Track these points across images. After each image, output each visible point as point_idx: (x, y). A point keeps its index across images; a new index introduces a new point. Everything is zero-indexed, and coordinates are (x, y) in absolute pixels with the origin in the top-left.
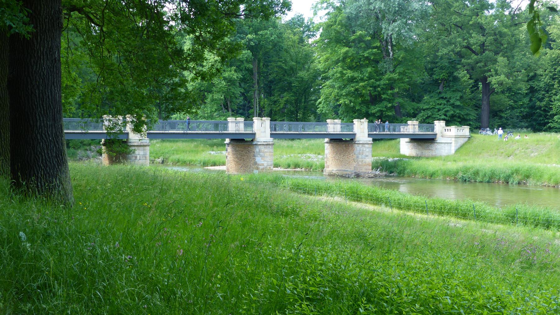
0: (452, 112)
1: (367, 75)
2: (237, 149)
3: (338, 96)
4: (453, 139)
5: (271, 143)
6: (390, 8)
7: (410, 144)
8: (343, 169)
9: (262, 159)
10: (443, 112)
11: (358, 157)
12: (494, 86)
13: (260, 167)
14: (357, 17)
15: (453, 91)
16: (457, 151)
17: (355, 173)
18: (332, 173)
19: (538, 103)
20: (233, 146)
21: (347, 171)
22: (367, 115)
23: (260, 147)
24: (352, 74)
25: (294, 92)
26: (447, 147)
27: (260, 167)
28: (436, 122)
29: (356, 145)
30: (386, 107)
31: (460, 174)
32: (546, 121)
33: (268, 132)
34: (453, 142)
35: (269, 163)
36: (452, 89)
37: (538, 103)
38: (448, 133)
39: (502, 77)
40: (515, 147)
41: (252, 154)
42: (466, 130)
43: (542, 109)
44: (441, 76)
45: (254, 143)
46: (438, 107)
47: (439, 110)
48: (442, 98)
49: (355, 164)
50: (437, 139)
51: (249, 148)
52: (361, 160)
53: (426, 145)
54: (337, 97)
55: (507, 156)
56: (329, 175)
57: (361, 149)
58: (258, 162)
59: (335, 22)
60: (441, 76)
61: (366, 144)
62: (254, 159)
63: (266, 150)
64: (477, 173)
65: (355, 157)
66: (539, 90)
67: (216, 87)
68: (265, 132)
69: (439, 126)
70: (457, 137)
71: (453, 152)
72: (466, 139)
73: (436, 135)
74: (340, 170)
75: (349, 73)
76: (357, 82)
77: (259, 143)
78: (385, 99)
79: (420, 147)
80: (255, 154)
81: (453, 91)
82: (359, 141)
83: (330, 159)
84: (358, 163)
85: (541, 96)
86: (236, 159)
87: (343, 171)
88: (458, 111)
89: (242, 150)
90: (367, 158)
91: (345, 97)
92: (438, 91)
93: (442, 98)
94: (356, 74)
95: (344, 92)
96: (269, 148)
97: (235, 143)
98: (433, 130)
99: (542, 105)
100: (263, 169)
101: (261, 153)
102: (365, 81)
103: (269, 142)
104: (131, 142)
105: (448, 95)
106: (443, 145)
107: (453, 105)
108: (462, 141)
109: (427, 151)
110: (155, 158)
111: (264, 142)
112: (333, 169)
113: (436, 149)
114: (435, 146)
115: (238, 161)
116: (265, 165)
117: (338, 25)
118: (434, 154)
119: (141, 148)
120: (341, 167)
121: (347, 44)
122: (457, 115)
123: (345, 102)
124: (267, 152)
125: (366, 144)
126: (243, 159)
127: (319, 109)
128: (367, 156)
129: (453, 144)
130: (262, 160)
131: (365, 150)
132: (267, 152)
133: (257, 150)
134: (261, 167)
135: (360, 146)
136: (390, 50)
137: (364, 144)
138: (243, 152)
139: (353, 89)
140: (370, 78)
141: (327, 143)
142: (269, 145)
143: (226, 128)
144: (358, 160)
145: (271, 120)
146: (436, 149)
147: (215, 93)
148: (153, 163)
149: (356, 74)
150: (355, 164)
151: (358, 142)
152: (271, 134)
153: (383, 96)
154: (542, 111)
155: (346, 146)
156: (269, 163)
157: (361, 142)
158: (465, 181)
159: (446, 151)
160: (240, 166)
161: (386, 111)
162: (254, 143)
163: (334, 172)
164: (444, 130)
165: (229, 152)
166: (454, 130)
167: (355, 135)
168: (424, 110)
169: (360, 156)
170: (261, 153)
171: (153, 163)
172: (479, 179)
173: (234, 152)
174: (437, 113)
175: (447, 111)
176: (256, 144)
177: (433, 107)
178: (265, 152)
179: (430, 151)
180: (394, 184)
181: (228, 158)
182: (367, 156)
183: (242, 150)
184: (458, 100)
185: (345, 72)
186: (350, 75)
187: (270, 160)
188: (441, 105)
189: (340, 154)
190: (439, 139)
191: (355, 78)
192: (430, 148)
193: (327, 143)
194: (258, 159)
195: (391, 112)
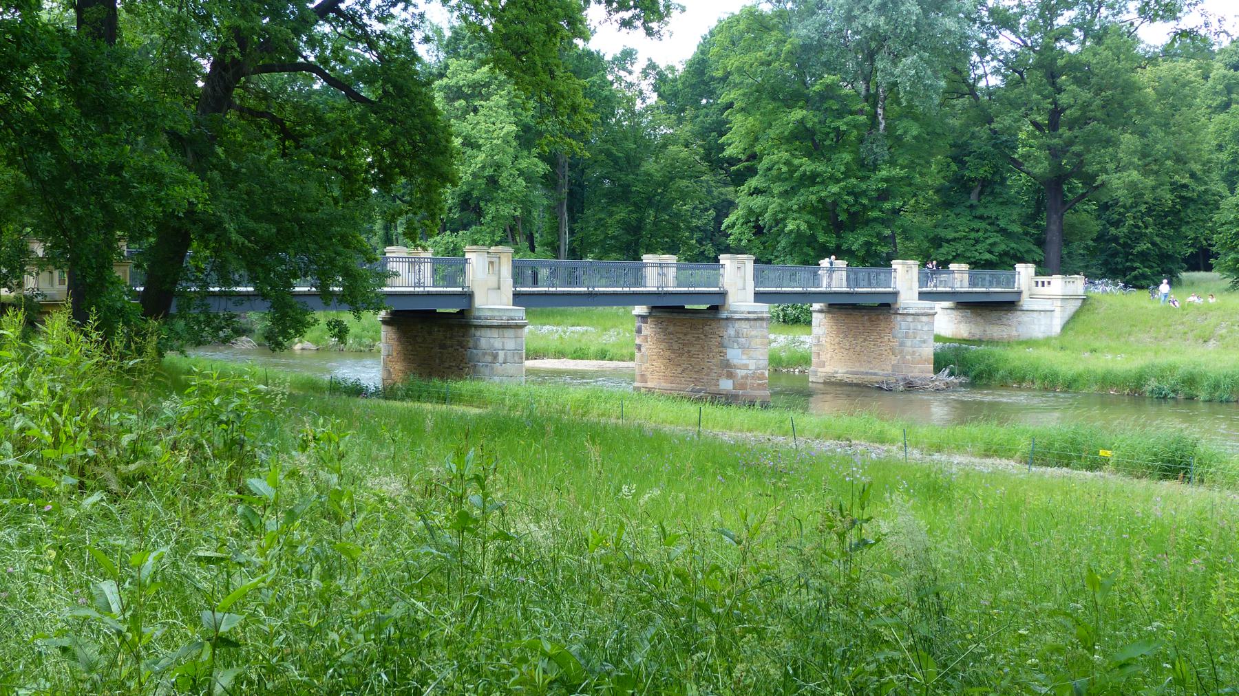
0: (1003, 247)
1: (843, 168)
2: (671, 328)
3: (781, 211)
4: (1059, 303)
5: (765, 315)
6: (896, 28)
7: (955, 313)
8: (862, 370)
9: (743, 353)
10: (985, 246)
11: (902, 344)
12: (1119, 192)
13: (738, 371)
14: (819, 47)
15: (1002, 203)
16: (1065, 328)
17: (905, 379)
18: (833, 379)
19: (1113, 230)
20: (659, 322)
21: (875, 374)
22: (839, 253)
23: (737, 324)
24: (813, 167)
25: (635, 204)
26: (1043, 320)
27: (738, 371)
28: (1020, 267)
29: (899, 318)
30: (878, 235)
31: (1153, 384)
32: (1128, 264)
33: (508, 288)
34: (1058, 310)
35: (761, 362)
36: (1001, 200)
37: (1113, 230)
38: (1046, 290)
39: (1135, 175)
40: (1212, 321)
41: (714, 342)
42: (1077, 284)
43: (1121, 241)
44: (981, 172)
45: (724, 315)
46: (973, 235)
47: (977, 241)
48: (981, 218)
49: (894, 360)
50: (1021, 303)
51: (707, 328)
52: (910, 350)
53: (995, 314)
54: (780, 216)
55: (1201, 341)
56: (825, 383)
57: (912, 326)
58: (734, 361)
59: (778, 55)
60: (981, 172)
61: (922, 315)
62: (724, 354)
63: (753, 333)
64: (1191, 381)
65: (895, 343)
66: (1111, 205)
67: (503, 191)
68: (499, 288)
69: (1025, 273)
70: (1065, 298)
71: (1057, 329)
72: (1079, 303)
73: (1019, 293)
74: (856, 373)
75: (807, 165)
76: (823, 182)
77: (737, 316)
78: (875, 220)
79: (979, 319)
80: (726, 342)
81: (1002, 203)
82: (905, 308)
83: (829, 347)
84: (903, 357)
85: (1116, 217)
86: (667, 354)
87: (862, 373)
88: (1013, 245)
89: (685, 331)
90: (924, 345)
91: (795, 215)
92: (968, 204)
93: (981, 218)
94: (820, 167)
95: (794, 203)
96: (761, 327)
97: (667, 315)
98: (1010, 281)
99: (1121, 235)
100: (746, 377)
101: (742, 340)
102: (838, 181)
103: (762, 312)
104: (479, 318)
105: (993, 211)
106: (1035, 314)
107: (1003, 231)
108: (1074, 306)
109: (996, 328)
110: (374, 340)
111: (749, 313)
112: (836, 369)
113: (1020, 323)
114: (1015, 318)
115: (673, 356)
116: (752, 367)
117: (785, 60)
118: (1014, 333)
119: (510, 333)
120: (857, 364)
121: (808, 102)
122: (1012, 251)
123: (798, 226)
124: (756, 337)
125: (922, 315)
126: (689, 352)
127: (732, 237)
128: (924, 342)
129: (1058, 313)
130: (744, 357)
131: (920, 327)
132: (756, 337)
133: (731, 332)
134: (741, 373)
135: (910, 319)
136: (880, 118)
137: (918, 315)
138: (688, 337)
139: (814, 197)
140: (847, 175)
141: (820, 311)
142: (761, 319)
143: (640, 281)
144: (902, 351)
145: (756, 262)
146: (1020, 323)
147: (501, 203)
148: (370, 350)
149: (820, 167)
150: (894, 360)
151: (905, 312)
152: (920, 293)
153: (874, 214)
154: (1119, 244)
155: (870, 320)
156: (761, 362)
157: (911, 311)
158: (1165, 397)
159: (1043, 328)
160: (680, 370)
161: (879, 244)
162: (724, 315)
163: (839, 376)
164: (1034, 284)
165: (646, 337)
166: (1057, 284)
167: (723, 295)
168: (948, 241)
169: (909, 343)
170: (742, 340)
171: (370, 350)
172: (1203, 395)
173: (662, 336)
174: (973, 249)
175: (994, 244)
176: (727, 319)
177: (965, 236)
178: (751, 337)
179: (1003, 328)
180: (993, 406)
181: (643, 349)
182: (924, 342)
183: (685, 331)
184: (1014, 221)
185: (796, 162)
186: (808, 169)
187: (762, 355)
188: (978, 231)
189: (855, 337)
190: (1026, 302)
191: (819, 175)
192: (1005, 321)
193: (820, 311)
194: (734, 355)
195: (885, 245)
